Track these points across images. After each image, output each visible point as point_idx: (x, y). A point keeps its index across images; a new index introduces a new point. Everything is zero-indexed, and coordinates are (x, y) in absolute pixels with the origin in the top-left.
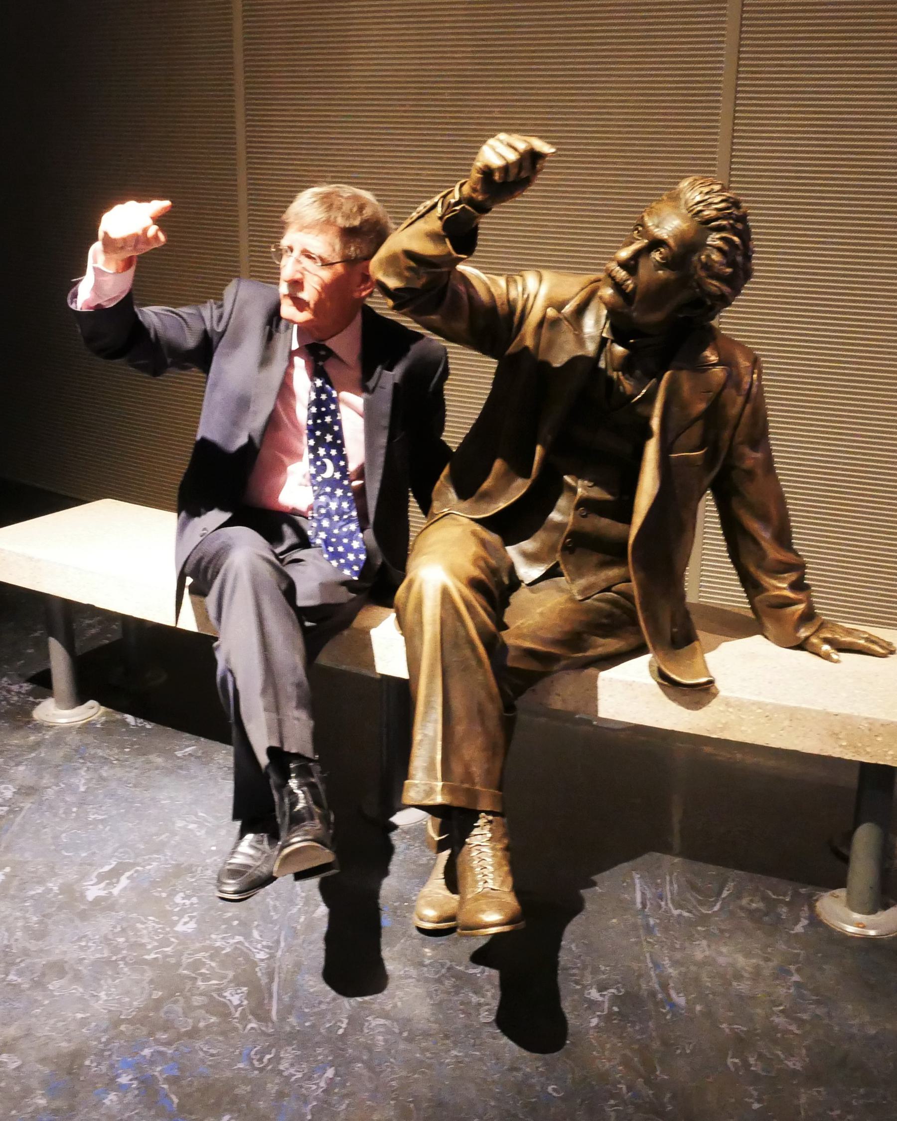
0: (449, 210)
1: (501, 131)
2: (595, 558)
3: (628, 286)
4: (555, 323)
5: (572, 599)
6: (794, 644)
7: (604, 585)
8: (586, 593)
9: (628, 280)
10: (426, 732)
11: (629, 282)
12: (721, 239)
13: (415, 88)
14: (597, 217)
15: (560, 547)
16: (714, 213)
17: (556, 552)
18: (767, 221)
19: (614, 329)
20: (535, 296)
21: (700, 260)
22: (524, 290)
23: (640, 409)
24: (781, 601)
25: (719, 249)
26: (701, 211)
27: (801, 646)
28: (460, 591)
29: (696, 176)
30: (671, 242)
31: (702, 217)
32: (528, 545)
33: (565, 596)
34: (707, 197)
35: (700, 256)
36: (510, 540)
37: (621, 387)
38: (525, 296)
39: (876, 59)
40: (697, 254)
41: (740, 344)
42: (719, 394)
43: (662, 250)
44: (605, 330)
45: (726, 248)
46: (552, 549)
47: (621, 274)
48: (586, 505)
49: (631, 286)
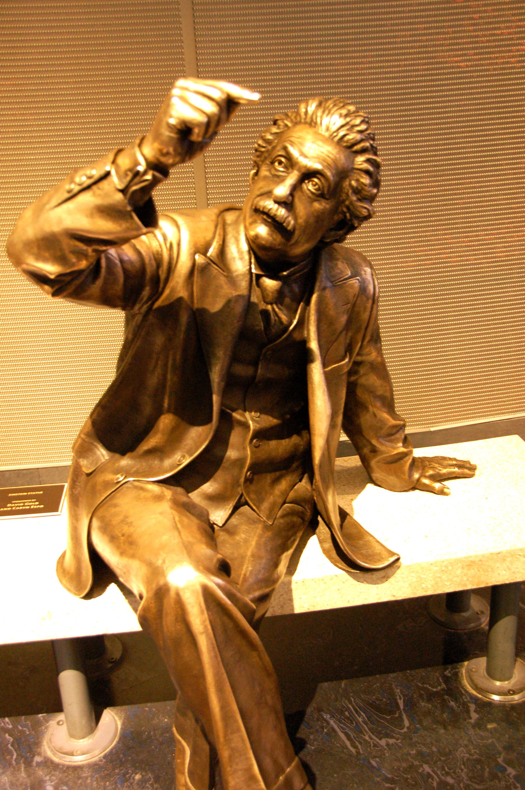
0: (137, 180)
1: (176, 78)
2: (269, 478)
3: (289, 222)
4: (204, 269)
5: (266, 528)
6: (411, 487)
7: (281, 501)
8: (270, 514)
10: (233, 745)
11: (290, 218)
12: (368, 161)
14: (480, 202)
15: (242, 480)
16: (359, 137)
17: (239, 486)
19: (260, 262)
20: (179, 245)
21: (350, 185)
22: (165, 239)
23: (297, 336)
24: (397, 457)
25: (367, 172)
26: (345, 136)
27: (416, 486)
28: (218, 585)
29: (336, 97)
30: (328, 173)
31: (347, 141)
32: (208, 487)
33: (260, 526)
35: (350, 181)
36: (189, 489)
38: (168, 245)
40: (348, 180)
41: (359, 253)
42: (354, 305)
43: (316, 180)
44: (253, 266)
45: (371, 169)
46: (235, 483)
47: (282, 212)
49: (292, 222)
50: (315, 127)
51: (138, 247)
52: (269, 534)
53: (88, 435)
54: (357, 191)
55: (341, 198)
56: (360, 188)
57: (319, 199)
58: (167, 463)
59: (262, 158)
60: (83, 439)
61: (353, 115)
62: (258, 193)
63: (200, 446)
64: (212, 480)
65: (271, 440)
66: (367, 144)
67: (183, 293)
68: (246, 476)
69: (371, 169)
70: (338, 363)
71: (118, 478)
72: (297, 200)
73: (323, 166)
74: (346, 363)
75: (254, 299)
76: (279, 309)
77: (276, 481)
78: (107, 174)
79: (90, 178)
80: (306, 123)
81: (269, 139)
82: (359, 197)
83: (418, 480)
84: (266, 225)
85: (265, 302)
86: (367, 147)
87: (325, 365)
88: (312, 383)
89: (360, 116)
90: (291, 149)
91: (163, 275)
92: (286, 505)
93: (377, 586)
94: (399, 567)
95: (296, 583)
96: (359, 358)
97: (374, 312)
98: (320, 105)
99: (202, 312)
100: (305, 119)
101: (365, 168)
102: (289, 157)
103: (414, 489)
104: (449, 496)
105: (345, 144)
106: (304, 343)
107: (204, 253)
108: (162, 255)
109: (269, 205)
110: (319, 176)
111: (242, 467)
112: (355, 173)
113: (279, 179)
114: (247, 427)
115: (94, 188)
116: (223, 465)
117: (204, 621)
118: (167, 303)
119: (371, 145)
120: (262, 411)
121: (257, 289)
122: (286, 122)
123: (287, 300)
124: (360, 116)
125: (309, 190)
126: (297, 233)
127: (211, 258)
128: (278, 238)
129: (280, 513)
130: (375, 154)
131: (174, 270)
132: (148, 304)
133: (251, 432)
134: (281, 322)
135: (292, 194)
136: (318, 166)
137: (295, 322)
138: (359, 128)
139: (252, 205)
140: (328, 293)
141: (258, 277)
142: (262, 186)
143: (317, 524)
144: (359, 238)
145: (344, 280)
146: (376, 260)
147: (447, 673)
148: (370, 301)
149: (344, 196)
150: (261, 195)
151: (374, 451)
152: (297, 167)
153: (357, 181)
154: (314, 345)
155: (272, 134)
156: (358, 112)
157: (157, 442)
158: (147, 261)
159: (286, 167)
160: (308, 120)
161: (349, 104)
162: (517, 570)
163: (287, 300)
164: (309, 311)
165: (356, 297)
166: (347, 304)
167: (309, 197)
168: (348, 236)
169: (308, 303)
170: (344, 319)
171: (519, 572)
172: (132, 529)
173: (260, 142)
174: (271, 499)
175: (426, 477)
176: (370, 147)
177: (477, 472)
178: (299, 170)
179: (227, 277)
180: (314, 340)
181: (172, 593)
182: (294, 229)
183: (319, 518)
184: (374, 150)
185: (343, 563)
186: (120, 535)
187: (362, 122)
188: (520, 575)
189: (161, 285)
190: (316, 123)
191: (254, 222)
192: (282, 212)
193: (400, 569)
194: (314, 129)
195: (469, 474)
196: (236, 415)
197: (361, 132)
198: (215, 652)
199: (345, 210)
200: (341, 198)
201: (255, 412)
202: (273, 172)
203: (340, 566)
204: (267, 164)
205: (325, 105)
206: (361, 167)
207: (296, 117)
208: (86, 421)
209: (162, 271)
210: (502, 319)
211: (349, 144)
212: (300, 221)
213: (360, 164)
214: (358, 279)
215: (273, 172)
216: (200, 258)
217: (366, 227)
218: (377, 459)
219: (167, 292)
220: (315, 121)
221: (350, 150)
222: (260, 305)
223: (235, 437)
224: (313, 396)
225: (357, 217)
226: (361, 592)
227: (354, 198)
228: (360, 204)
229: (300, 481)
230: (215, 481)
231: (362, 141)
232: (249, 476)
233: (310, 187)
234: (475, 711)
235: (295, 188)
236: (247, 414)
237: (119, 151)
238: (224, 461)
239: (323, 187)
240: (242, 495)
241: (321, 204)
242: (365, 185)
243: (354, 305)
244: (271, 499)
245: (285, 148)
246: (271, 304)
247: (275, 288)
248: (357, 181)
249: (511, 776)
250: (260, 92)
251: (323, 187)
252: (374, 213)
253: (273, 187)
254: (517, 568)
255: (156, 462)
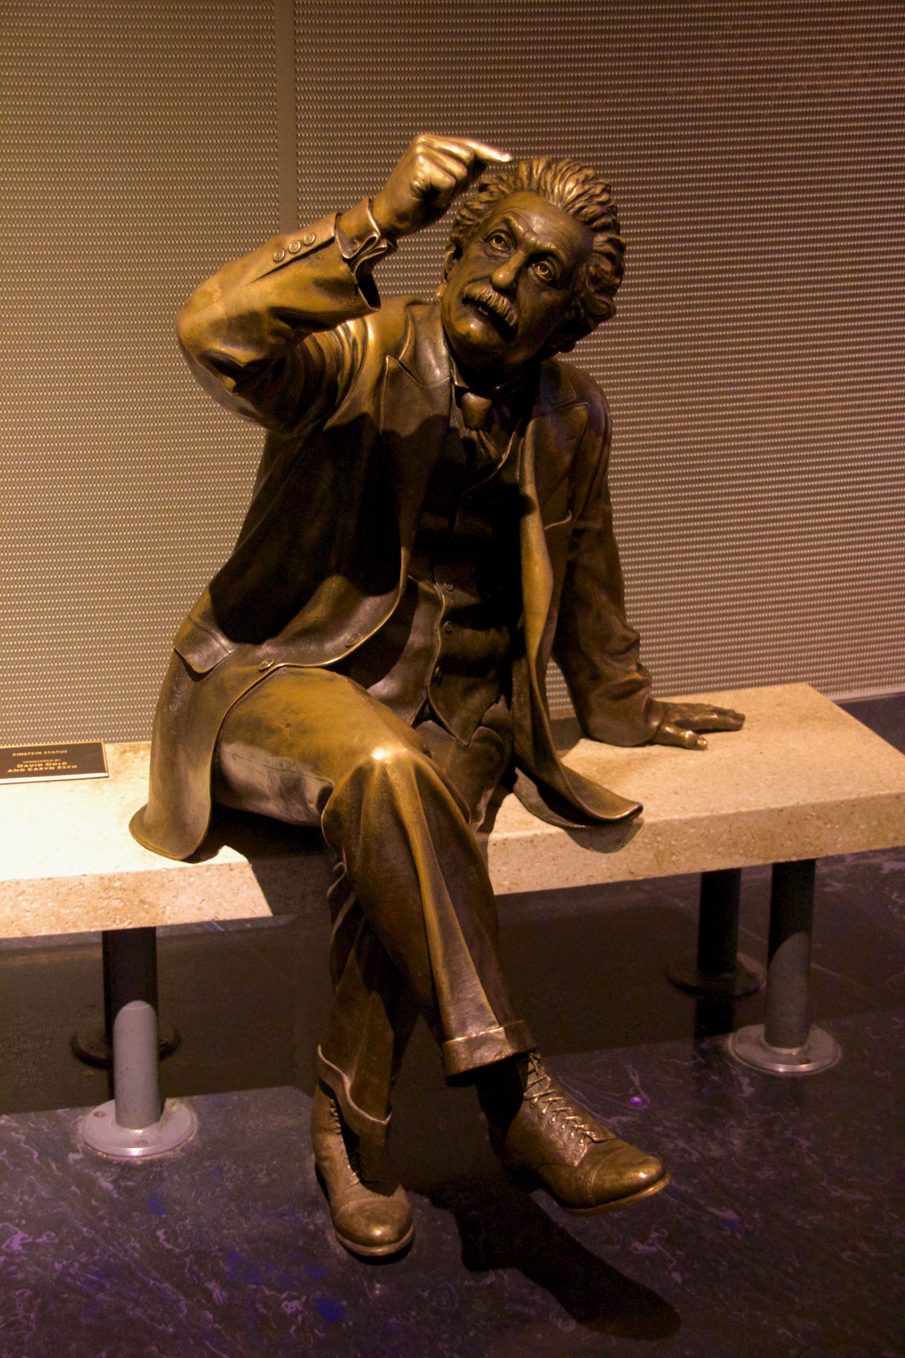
2: (461, 683)
3: (512, 317)
4: (395, 376)
7: (475, 718)
9: (510, 309)
12: (610, 241)
13: (870, 643)
15: (428, 679)
16: (596, 209)
18: (799, 411)
21: (587, 271)
25: (609, 256)
26: (582, 208)
29: (568, 157)
30: (562, 255)
34: (587, 187)
37: (493, 443)
38: (351, 341)
39: (842, 181)
42: (581, 441)
45: (614, 252)
46: (419, 684)
47: (503, 303)
48: (456, 616)
50: (545, 196)
51: (320, 342)
52: (464, 755)
53: (204, 616)
54: (595, 280)
55: (576, 289)
56: (599, 276)
57: (549, 288)
58: (329, 646)
59: (470, 234)
60: (196, 624)
61: (591, 182)
62: (470, 278)
63: (380, 620)
64: (387, 676)
65: (466, 627)
66: (609, 220)
67: (367, 407)
68: (434, 673)
69: (614, 252)
70: (559, 521)
71: (265, 665)
72: (521, 289)
73: (557, 245)
74: (569, 522)
75: (455, 423)
76: (487, 438)
77: (469, 691)
78: (332, 241)
79: (304, 244)
80: (530, 190)
81: (478, 210)
82: (598, 289)
83: (659, 728)
84: (480, 320)
85: (467, 426)
86: (610, 223)
87: (545, 521)
88: (527, 541)
89: (600, 183)
90: (514, 222)
91: (341, 380)
92: (481, 728)
93: (608, 855)
94: (640, 826)
95: (495, 845)
96: (582, 525)
97: (605, 454)
98: (548, 167)
99: (390, 435)
100: (529, 185)
101: (606, 251)
102: (512, 233)
103: (651, 742)
104: (706, 752)
105: (582, 219)
106: (516, 489)
107: (396, 353)
108: (343, 355)
109: (486, 292)
110: (550, 258)
111: (429, 658)
112: (594, 257)
113: (500, 263)
114: (437, 603)
115: (312, 256)
116: (403, 655)
117: (418, 809)
118: (345, 421)
119: (613, 221)
120: (459, 583)
121: (457, 409)
122: (501, 187)
123: (495, 428)
124: (600, 183)
125: (537, 276)
126: (520, 330)
127: (403, 363)
128: (495, 338)
129: (474, 735)
130: (618, 233)
131: (357, 377)
132: (315, 424)
133: (443, 609)
134: (489, 458)
135: (516, 280)
136: (550, 245)
137: (504, 457)
138: (600, 199)
139: (461, 293)
140: (549, 421)
141: (460, 392)
142: (469, 270)
143: (515, 777)
144: (619, 328)
145: (568, 405)
146: (610, 385)
147: (705, 1045)
148: (601, 439)
149: (579, 285)
150: (474, 281)
151: (596, 677)
152: (523, 246)
153: (597, 266)
154: (530, 490)
155: (481, 203)
156: (597, 179)
157: (316, 617)
158: (328, 361)
159: (507, 246)
160: (534, 185)
161: (588, 167)
162: (807, 840)
163: (495, 428)
164: (524, 444)
165: (583, 430)
166: (572, 438)
167: (537, 285)
168: (578, 343)
169: (522, 433)
170: (567, 458)
171: (811, 844)
172: (302, 716)
173: (465, 212)
174: (463, 714)
175: (670, 724)
176: (612, 223)
177: (746, 725)
178: (526, 250)
179: (422, 389)
180: (530, 482)
181: (377, 772)
182: (517, 324)
183: (518, 771)
184: (615, 227)
185: (561, 818)
186: (283, 726)
187: (603, 191)
188: (812, 848)
189: (339, 395)
190: (545, 191)
191: (465, 315)
192: (503, 303)
193: (642, 828)
194: (543, 199)
195: (733, 725)
196: (423, 586)
197: (601, 204)
198: (431, 849)
199: (579, 304)
200: (576, 289)
201: (448, 583)
202: (490, 251)
203: (557, 821)
204: (480, 242)
205: (556, 167)
206: (602, 248)
207: (514, 182)
208: (200, 599)
209: (342, 376)
210: (801, 217)
211: (587, 219)
212: (525, 315)
213: (600, 246)
214: (586, 405)
215: (490, 251)
216: (391, 362)
217: (605, 328)
218: (598, 691)
219: (345, 405)
220: (543, 188)
221: (589, 227)
222: (461, 432)
223: (419, 619)
224: (528, 560)
225: (593, 316)
226: (585, 865)
227: (592, 289)
228: (598, 297)
229: (497, 702)
230: (392, 677)
231: (603, 215)
232: (438, 673)
233: (537, 272)
234: (750, 1084)
235: (521, 272)
236: (437, 587)
237: (339, 215)
238: (406, 649)
239: (556, 273)
240: (427, 702)
241: (550, 295)
242: (606, 273)
243: (581, 441)
244: (463, 714)
245: (507, 222)
246: (477, 430)
247: (483, 408)
248: (597, 266)
249: (803, 1147)
250: (512, 153)
251: (556, 273)
252: (615, 311)
253: (492, 271)
254: (808, 837)
255: (313, 648)
